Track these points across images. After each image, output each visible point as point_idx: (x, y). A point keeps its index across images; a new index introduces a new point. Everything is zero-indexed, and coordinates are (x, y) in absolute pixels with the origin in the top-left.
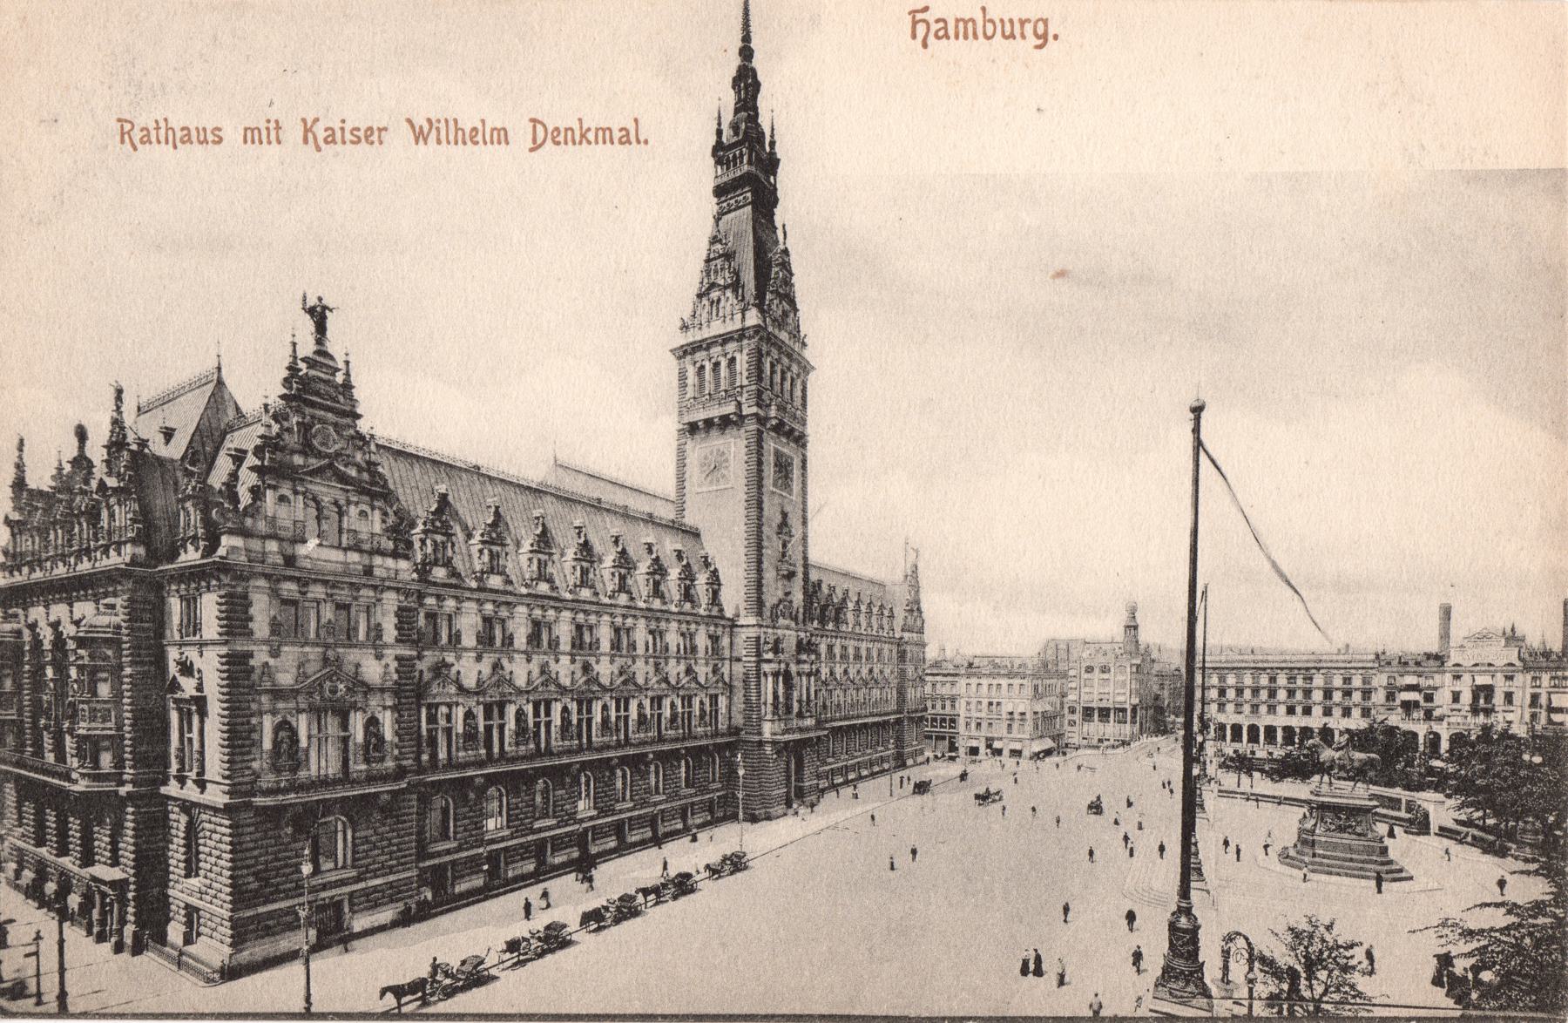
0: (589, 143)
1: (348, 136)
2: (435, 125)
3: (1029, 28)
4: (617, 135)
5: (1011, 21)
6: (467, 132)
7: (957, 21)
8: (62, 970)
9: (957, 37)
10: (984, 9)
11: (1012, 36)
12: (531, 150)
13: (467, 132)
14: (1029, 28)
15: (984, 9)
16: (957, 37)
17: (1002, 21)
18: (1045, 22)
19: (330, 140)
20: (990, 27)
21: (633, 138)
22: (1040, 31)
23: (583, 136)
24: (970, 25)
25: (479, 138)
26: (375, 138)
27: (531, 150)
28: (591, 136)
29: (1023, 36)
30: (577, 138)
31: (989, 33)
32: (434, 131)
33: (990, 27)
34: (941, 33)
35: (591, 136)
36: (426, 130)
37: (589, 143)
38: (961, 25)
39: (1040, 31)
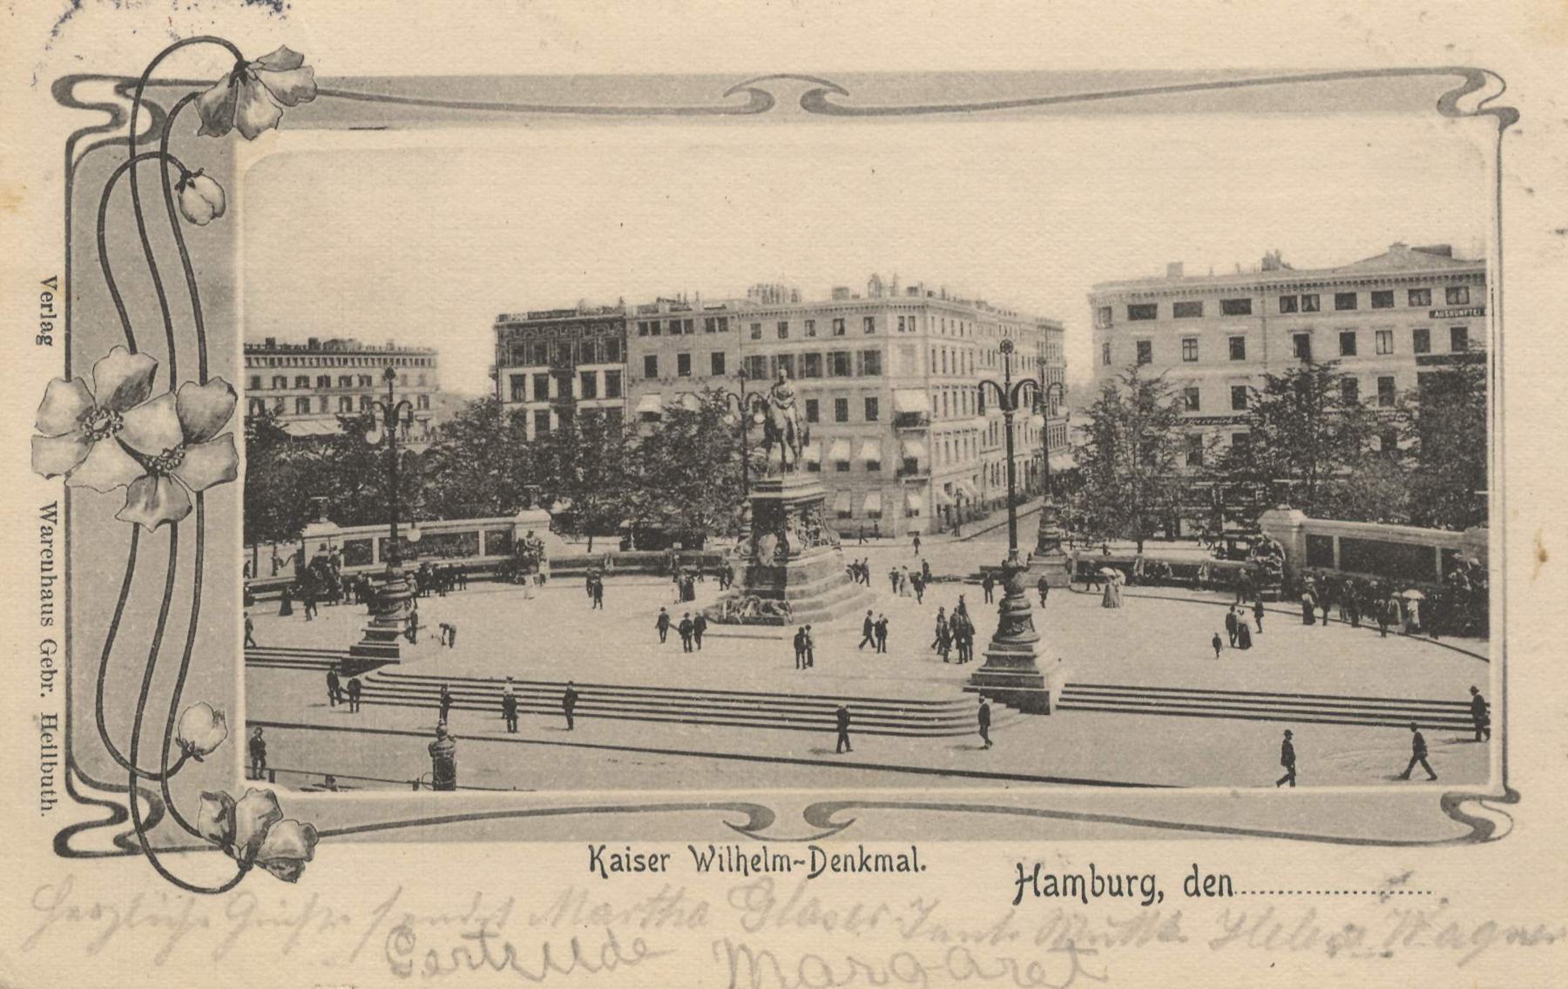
0: (869, 869)
1: (633, 864)
2: (718, 852)
3: (1136, 885)
4: (896, 862)
5: (1119, 878)
6: (749, 859)
7: (1065, 879)
8: (1505, 600)
9: (1065, 894)
10: (1092, 866)
11: (1120, 893)
12: (810, 877)
13: (749, 859)
14: (1136, 885)
15: (1092, 866)
16: (1065, 894)
17: (1110, 878)
18: (1153, 879)
19: (617, 866)
20: (1098, 883)
21: (911, 865)
22: (1148, 887)
23: (863, 863)
24: (1079, 882)
25: (761, 865)
26: (658, 865)
27: (810, 877)
28: (871, 863)
29: (1130, 894)
30: (857, 865)
31: (1098, 890)
32: (716, 860)
33: (1098, 883)
34: (1051, 890)
35: (871, 863)
36: (708, 857)
37: (869, 869)
38: (1070, 882)
39: (1148, 887)
